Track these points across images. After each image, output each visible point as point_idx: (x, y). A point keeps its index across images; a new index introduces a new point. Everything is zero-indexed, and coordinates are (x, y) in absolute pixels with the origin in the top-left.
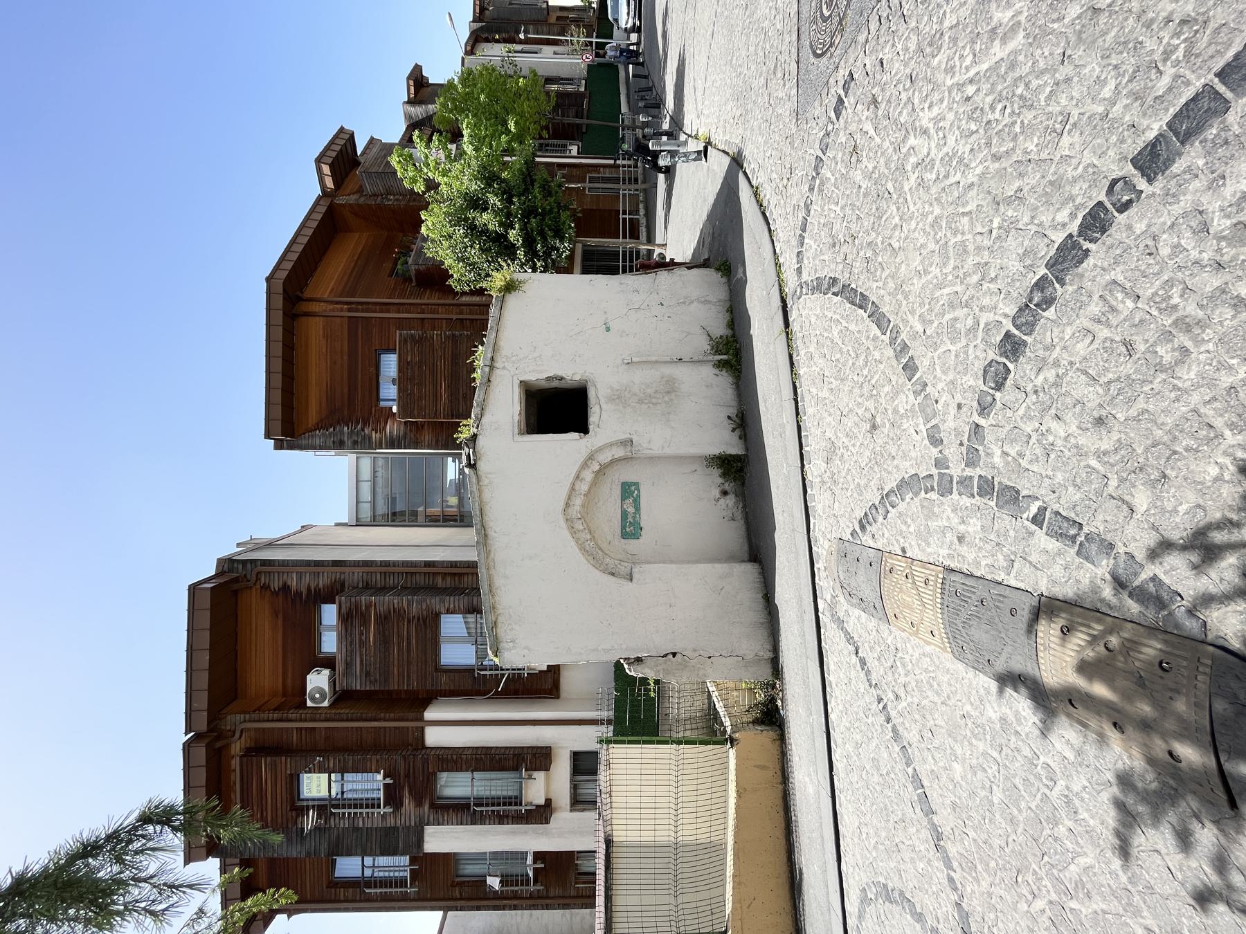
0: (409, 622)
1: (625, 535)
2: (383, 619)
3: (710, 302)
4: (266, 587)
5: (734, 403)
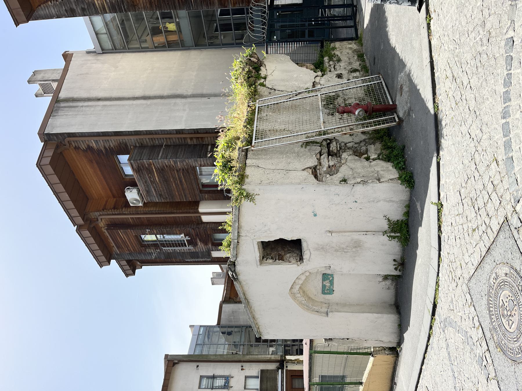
0: (177, 171)
1: (323, 293)
2: (161, 171)
3: (393, 201)
4: (77, 148)
5: (400, 254)
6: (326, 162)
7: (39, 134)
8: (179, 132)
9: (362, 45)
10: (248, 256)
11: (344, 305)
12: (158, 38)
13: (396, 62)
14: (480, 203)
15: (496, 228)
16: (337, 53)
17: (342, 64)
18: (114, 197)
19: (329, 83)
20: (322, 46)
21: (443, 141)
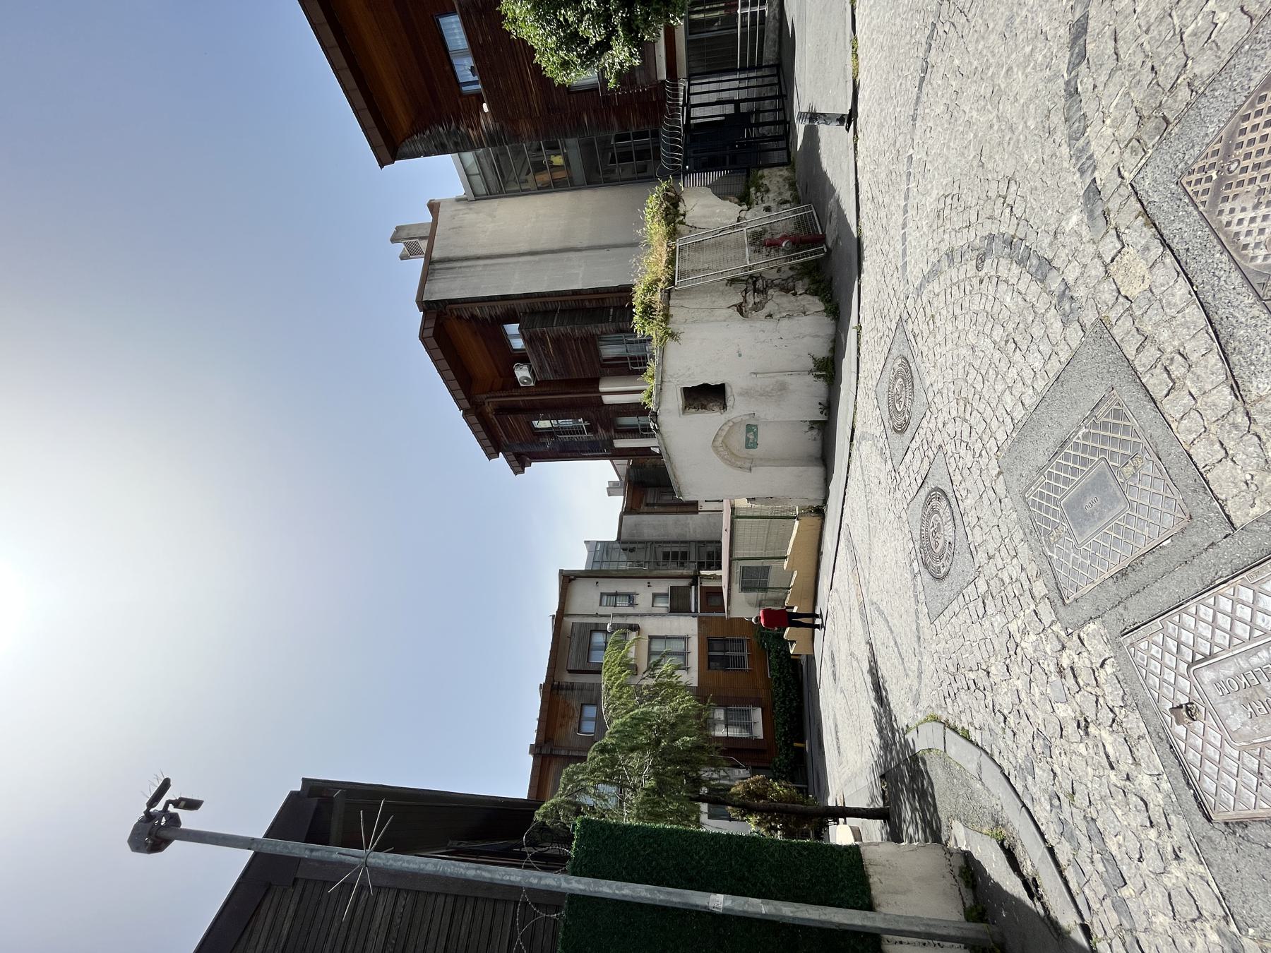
1: (747, 447)
2: (557, 341)
4: (459, 317)
7: (418, 302)
8: (575, 292)
16: (766, 182)
17: (771, 195)
19: (755, 217)
20: (748, 176)
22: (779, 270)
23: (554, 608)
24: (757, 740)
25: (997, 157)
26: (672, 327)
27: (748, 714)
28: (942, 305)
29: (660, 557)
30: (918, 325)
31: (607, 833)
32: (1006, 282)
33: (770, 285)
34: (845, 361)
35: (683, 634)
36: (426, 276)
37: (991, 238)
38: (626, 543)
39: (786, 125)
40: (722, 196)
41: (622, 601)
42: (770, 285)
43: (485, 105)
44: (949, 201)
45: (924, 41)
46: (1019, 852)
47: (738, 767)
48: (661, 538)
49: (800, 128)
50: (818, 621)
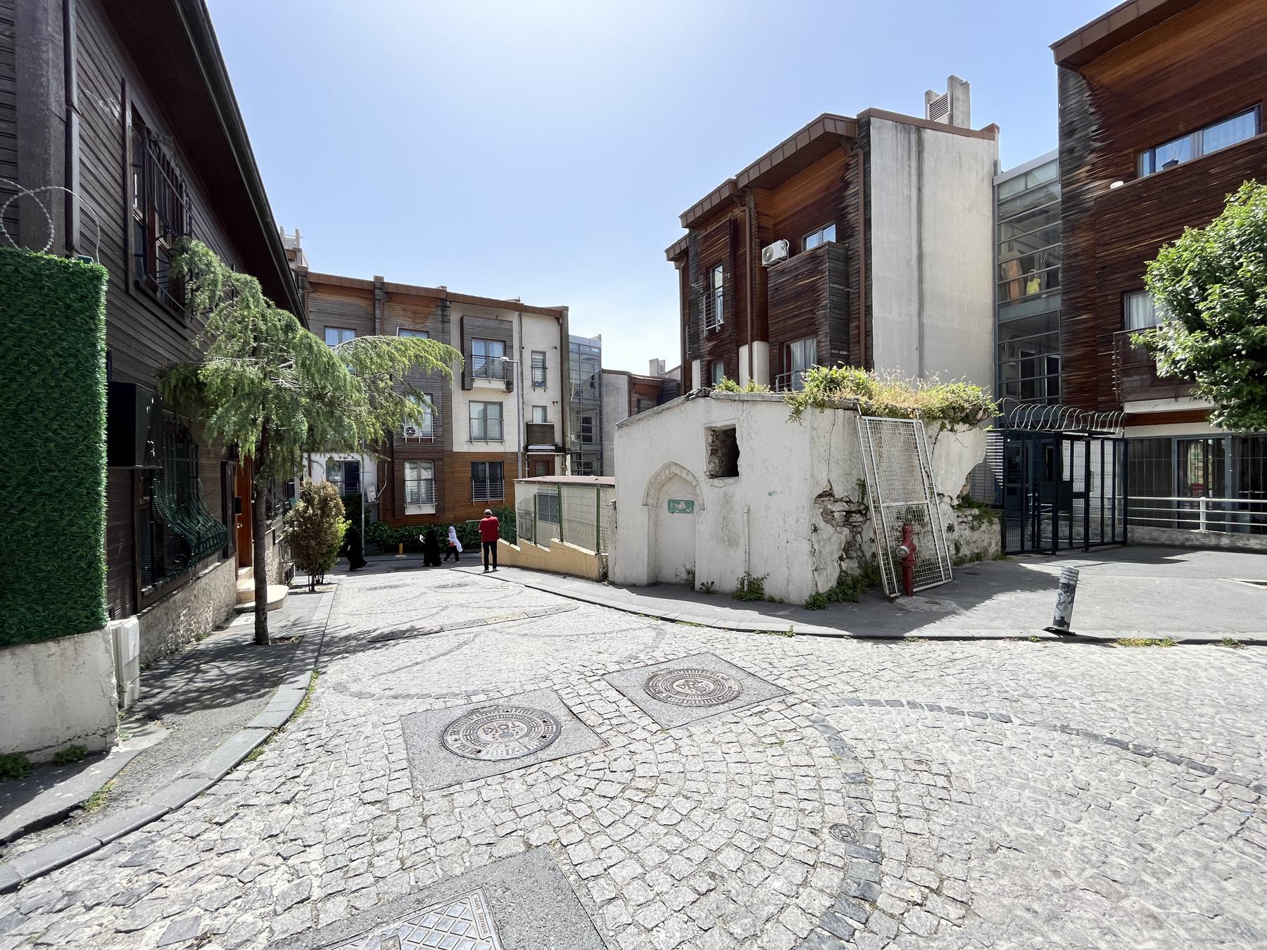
1: (670, 501)
2: (812, 288)
4: (847, 167)
6: (838, 509)
8: (869, 309)
9: (994, 559)
10: (719, 414)
11: (656, 525)
12: (1015, 268)
13: (971, 599)
14: (803, 672)
15: (780, 683)
16: (984, 527)
17: (967, 533)
18: (775, 225)
19: (942, 514)
20: (994, 507)
21: (870, 644)
22: (872, 541)
23: (526, 302)
24: (404, 509)
25: (1005, 881)
26: (808, 412)
27: (429, 500)
28: (794, 760)
29: (586, 415)
30: (777, 717)
31: (76, 305)
32: (805, 883)
33: (855, 530)
34: (754, 614)
35: (506, 437)
36: (902, 122)
37: (877, 858)
38: (599, 379)
39: (1053, 551)
40: (971, 476)
41: (538, 375)
42: (855, 530)
43: (1119, 184)
44: (941, 781)
45: (1184, 751)
46: (60, 830)
47: (378, 491)
48: (605, 416)
49: (1055, 568)
50: (491, 568)
